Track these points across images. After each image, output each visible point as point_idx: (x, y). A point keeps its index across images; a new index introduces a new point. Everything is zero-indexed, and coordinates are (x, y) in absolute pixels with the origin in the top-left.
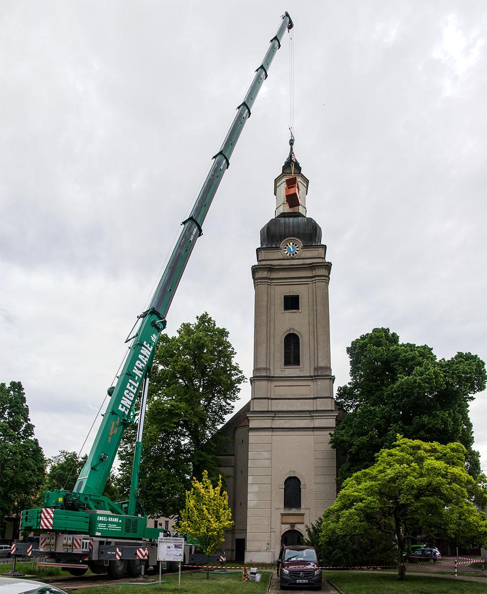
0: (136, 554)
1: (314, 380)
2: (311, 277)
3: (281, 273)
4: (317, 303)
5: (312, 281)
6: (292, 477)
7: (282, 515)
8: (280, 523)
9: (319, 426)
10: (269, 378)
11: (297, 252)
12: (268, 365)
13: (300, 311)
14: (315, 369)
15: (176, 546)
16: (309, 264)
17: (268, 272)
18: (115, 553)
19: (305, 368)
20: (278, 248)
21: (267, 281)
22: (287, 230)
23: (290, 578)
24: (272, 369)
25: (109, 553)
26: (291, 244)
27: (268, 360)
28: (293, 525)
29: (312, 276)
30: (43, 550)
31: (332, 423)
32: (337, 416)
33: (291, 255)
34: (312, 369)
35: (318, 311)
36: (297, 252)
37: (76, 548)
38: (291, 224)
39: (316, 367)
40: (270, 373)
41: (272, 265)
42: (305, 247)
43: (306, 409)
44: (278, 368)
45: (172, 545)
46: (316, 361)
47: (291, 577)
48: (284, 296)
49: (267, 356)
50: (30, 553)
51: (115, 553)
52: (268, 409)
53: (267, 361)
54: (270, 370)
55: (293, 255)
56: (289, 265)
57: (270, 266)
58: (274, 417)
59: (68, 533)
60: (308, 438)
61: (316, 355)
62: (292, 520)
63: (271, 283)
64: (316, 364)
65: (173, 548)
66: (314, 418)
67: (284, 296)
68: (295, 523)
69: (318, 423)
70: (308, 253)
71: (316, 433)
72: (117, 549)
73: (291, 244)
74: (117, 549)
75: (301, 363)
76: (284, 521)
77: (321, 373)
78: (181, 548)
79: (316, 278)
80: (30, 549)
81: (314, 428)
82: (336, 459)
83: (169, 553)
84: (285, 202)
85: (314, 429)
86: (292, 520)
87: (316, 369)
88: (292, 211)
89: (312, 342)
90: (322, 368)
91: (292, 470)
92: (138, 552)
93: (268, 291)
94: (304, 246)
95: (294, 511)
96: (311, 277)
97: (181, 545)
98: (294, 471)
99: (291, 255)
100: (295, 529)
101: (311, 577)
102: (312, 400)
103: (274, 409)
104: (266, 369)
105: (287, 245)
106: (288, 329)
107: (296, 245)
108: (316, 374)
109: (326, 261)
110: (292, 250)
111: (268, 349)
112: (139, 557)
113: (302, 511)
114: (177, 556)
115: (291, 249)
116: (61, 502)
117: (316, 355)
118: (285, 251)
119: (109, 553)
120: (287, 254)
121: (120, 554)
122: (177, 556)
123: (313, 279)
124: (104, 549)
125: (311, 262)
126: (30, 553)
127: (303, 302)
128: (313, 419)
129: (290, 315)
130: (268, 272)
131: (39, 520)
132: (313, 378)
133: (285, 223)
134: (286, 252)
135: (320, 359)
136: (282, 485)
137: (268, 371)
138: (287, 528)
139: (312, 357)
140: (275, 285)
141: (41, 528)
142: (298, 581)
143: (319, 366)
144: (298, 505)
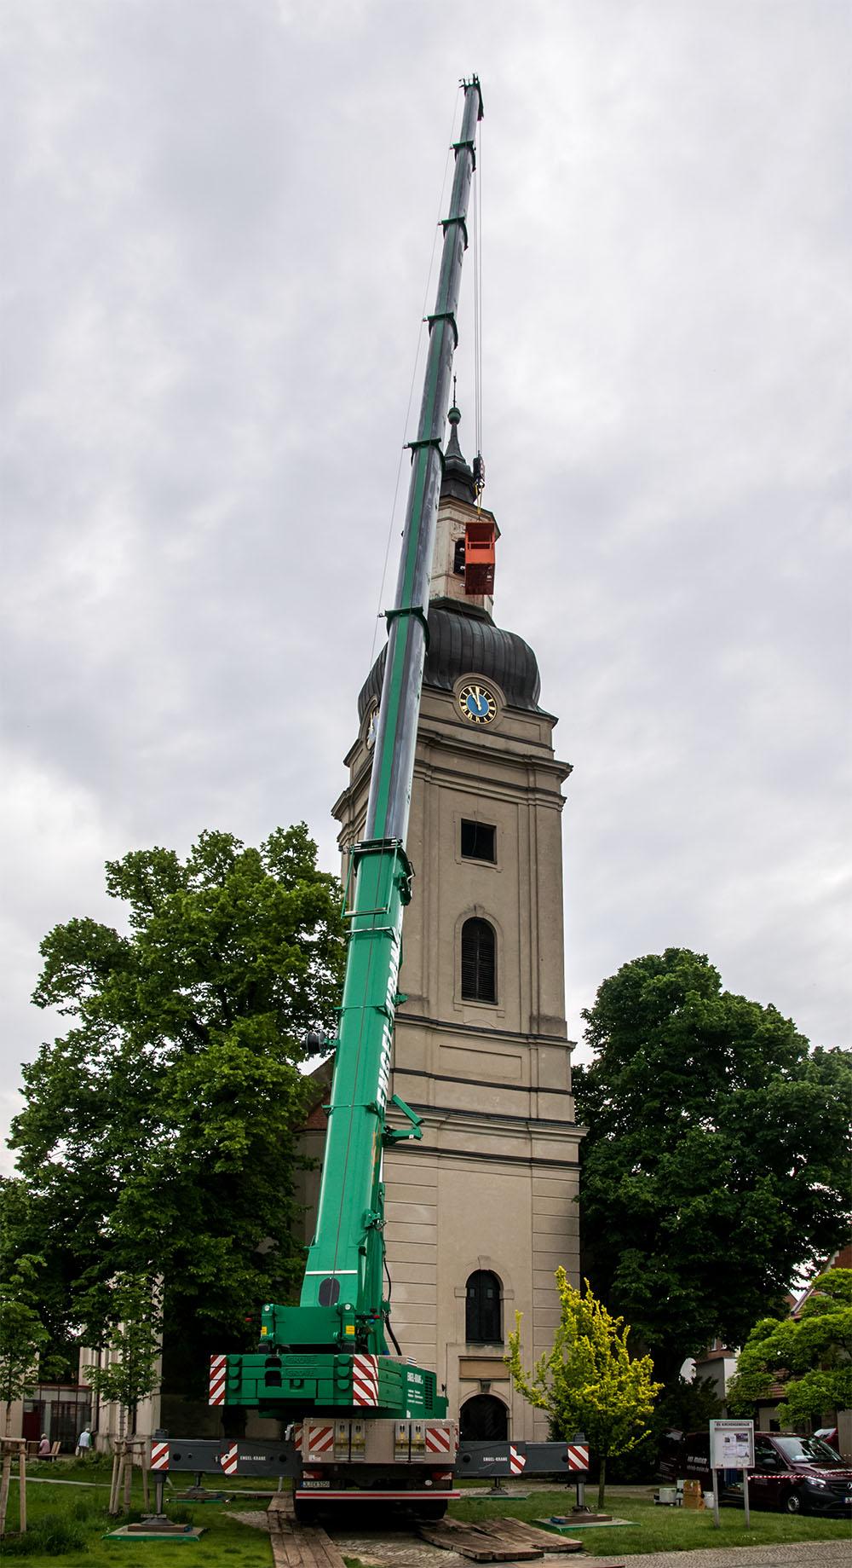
0: (566, 1459)
1: (532, 1046)
2: (527, 790)
3: (456, 760)
4: (539, 857)
5: (527, 800)
6: (484, 1271)
7: (462, 1359)
8: (457, 1380)
9: (544, 1157)
10: (430, 1025)
11: (490, 715)
12: (425, 990)
13: (498, 867)
14: (531, 1018)
15: (739, 1438)
16: (524, 756)
17: (426, 747)
18: (505, 1459)
19: (508, 1013)
20: (448, 692)
21: (424, 770)
22: (467, 652)
23: (832, 1495)
24: (433, 1001)
25: (486, 1459)
26: (478, 689)
27: (425, 978)
28: (485, 1383)
29: (525, 785)
30: (319, 1460)
31: (570, 1152)
32: (583, 1139)
33: (478, 719)
34: (526, 1017)
35: (542, 878)
36: (490, 715)
37: (435, 1450)
38: (478, 639)
39: (535, 1013)
40: (429, 1012)
41: (437, 734)
42: (510, 708)
43: (513, 1112)
44: (447, 1004)
45: (732, 1435)
46: (535, 1000)
47: (834, 1493)
48: (495, 827)
49: (531, 983)
50: (234, 1467)
51: (505, 1459)
52: (427, 1100)
53: (422, 978)
54: (428, 1002)
55: (482, 719)
56: (478, 746)
57: (433, 736)
58: (443, 1122)
59: (724, 1412)
60: (518, 1182)
61: (535, 984)
62: (484, 1371)
63: (431, 778)
64: (535, 1007)
65: (734, 1442)
66: (533, 1136)
67: (495, 827)
68: (489, 1380)
69: (541, 1149)
70: (515, 726)
71: (537, 1172)
72: (512, 1448)
73: (478, 689)
74: (512, 1448)
75: (500, 999)
76: (467, 1374)
77: (547, 1031)
78: (747, 1440)
79: (538, 796)
80: (230, 1456)
81: (532, 1160)
82: (580, 1236)
83: (729, 1452)
84: (451, 573)
85: (532, 1162)
86: (484, 1371)
87: (536, 1019)
88: (468, 603)
89: (525, 951)
90: (549, 1020)
91: (484, 1254)
92: (571, 1455)
93: (424, 797)
94: (509, 706)
95: (488, 1351)
96: (527, 790)
97: (746, 1435)
98: (487, 1258)
99: (478, 719)
100: (491, 1393)
101: (836, 1492)
102: (525, 1094)
103: (440, 1103)
104: (420, 999)
105: (467, 692)
106: (472, 905)
107: (488, 697)
108: (535, 1033)
109: (555, 759)
110: (480, 708)
111: (425, 949)
112: (573, 1465)
113: (507, 1353)
114: (741, 1457)
115: (479, 703)
116: (351, 1336)
117: (535, 984)
118: (463, 704)
119: (486, 1459)
120: (467, 712)
121: (522, 1460)
122: (741, 1457)
123: (530, 796)
124: (470, 1451)
125: (530, 753)
126: (234, 1467)
127: (504, 844)
128: (531, 1139)
129: (472, 869)
130: (426, 747)
131: (343, 1384)
132: (532, 1040)
133: (463, 630)
134: (465, 707)
135: (544, 997)
136: (461, 1289)
137: (426, 1005)
138: (472, 1390)
139: (525, 989)
140: (440, 786)
141: (356, 1403)
142: (847, 1499)
143: (542, 1012)
144: (494, 1336)
